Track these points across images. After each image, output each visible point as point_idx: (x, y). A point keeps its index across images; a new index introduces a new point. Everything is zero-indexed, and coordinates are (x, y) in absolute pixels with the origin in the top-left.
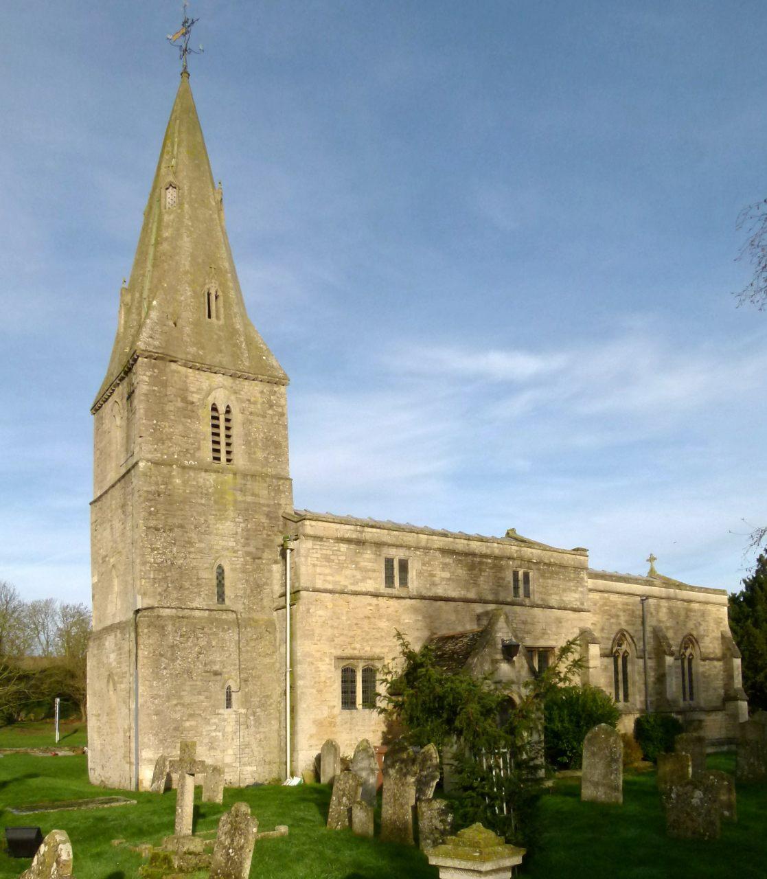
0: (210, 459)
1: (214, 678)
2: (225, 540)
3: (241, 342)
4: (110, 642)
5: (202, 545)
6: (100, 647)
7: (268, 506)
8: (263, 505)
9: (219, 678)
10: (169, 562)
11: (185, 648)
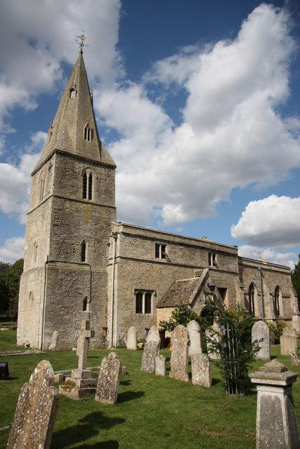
4: (32, 276)
5: (77, 234)
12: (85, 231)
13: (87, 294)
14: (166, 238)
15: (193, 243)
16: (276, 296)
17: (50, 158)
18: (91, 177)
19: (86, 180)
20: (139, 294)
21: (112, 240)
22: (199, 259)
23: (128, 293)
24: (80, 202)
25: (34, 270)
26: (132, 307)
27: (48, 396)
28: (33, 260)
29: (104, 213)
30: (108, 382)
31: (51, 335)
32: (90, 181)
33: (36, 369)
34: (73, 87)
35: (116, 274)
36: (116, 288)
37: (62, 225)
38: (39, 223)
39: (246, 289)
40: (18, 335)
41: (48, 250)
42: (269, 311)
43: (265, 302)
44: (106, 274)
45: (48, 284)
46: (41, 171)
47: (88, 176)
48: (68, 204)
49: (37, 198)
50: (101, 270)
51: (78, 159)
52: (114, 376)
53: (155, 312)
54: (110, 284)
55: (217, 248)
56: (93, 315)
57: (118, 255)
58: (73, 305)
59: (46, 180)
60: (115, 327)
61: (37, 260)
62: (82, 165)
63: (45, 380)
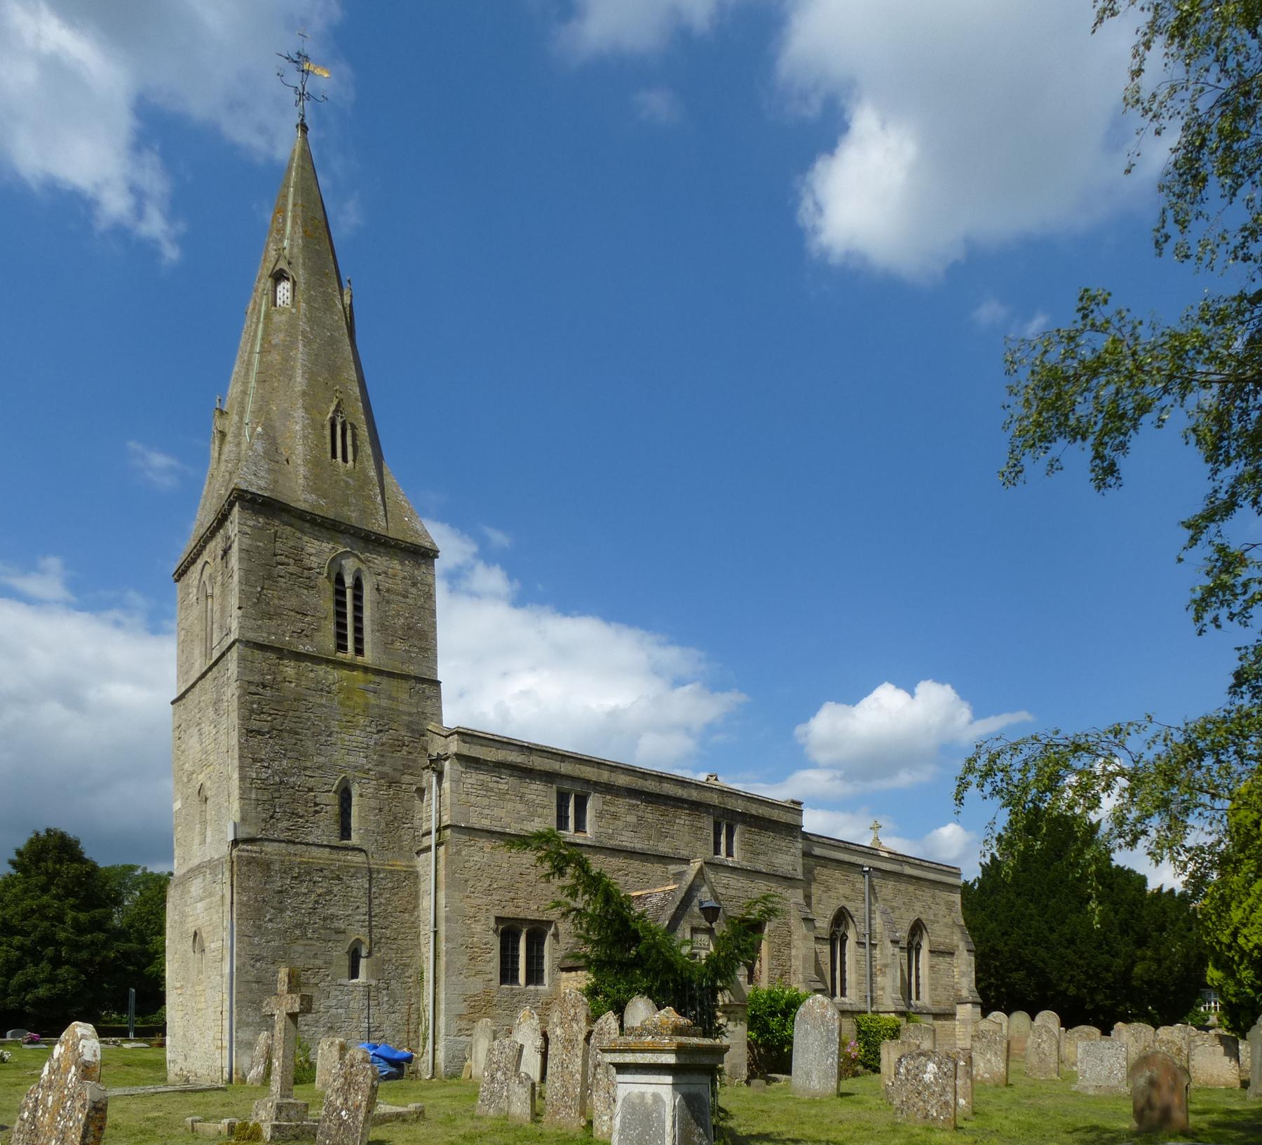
0: (332, 646)
1: (334, 937)
2: (351, 749)
3: (375, 495)
4: (196, 887)
5: (322, 759)
6: (185, 892)
7: (410, 714)
8: (404, 713)
9: (342, 937)
10: (277, 779)
11: (297, 894)
12: (351, 749)
13: (358, 932)
14: (589, 773)
15: (669, 789)
16: (912, 948)
17: (222, 519)
18: (358, 586)
19: (343, 594)
20: (508, 931)
21: (430, 778)
22: (688, 838)
23: (478, 928)
24: (328, 662)
25: (198, 870)
26: (488, 969)
27: (78, 1104)
28: (197, 840)
29: (402, 691)
30: (342, 1123)
31: (250, 1045)
32: (358, 598)
33: (58, 1046)
34: (283, 265)
35: (442, 873)
36: (442, 913)
37: (275, 732)
38: (207, 728)
39: (823, 924)
40: (169, 1056)
41: (236, 805)
42: (889, 990)
43: (878, 963)
44: (413, 876)
45: (241, 903)
46: (200, 563)
47: (349, 581)
48: (289, 669)
49: (197, 651)
50: (400, 864)
51: (402, 550)
52: (359, 1106)
53: (555, 983)
54: (427, 903)
55: (739, 806)
56: (378, 989)
57: (446, 820)
58: (319, 962)
59: (217, 591)
60: (442, 1021)
61: (208, 840)
62: (327, 546)
63: (73, 1068)
